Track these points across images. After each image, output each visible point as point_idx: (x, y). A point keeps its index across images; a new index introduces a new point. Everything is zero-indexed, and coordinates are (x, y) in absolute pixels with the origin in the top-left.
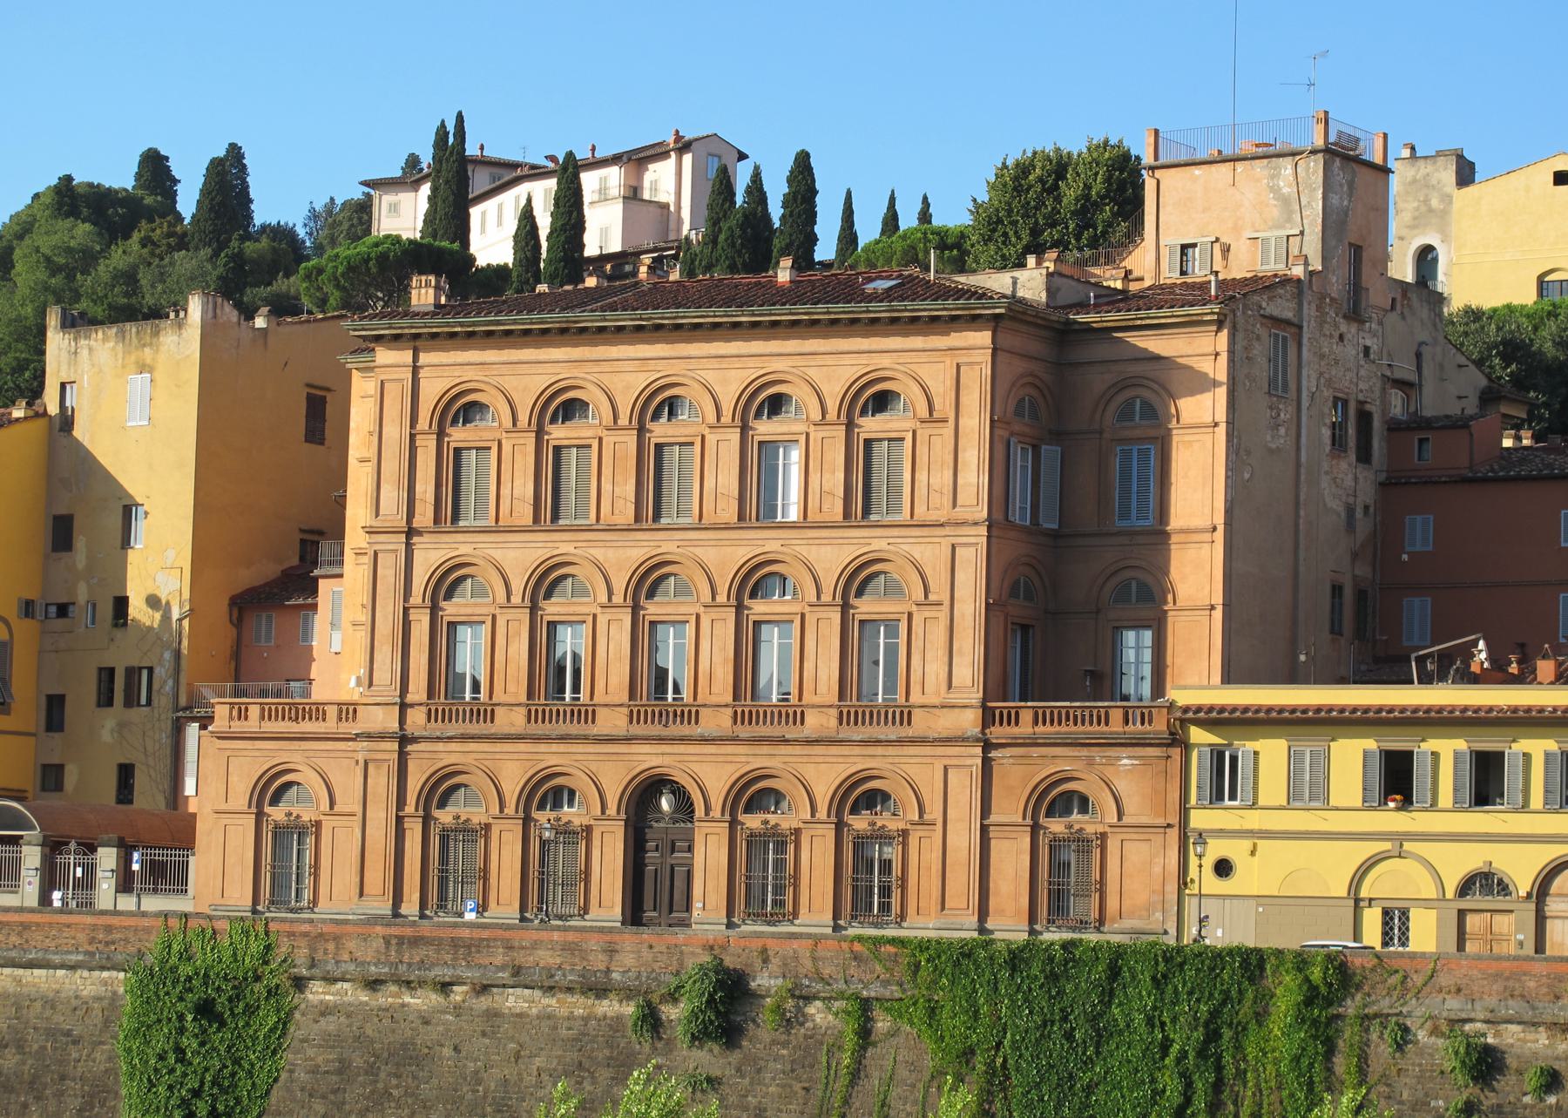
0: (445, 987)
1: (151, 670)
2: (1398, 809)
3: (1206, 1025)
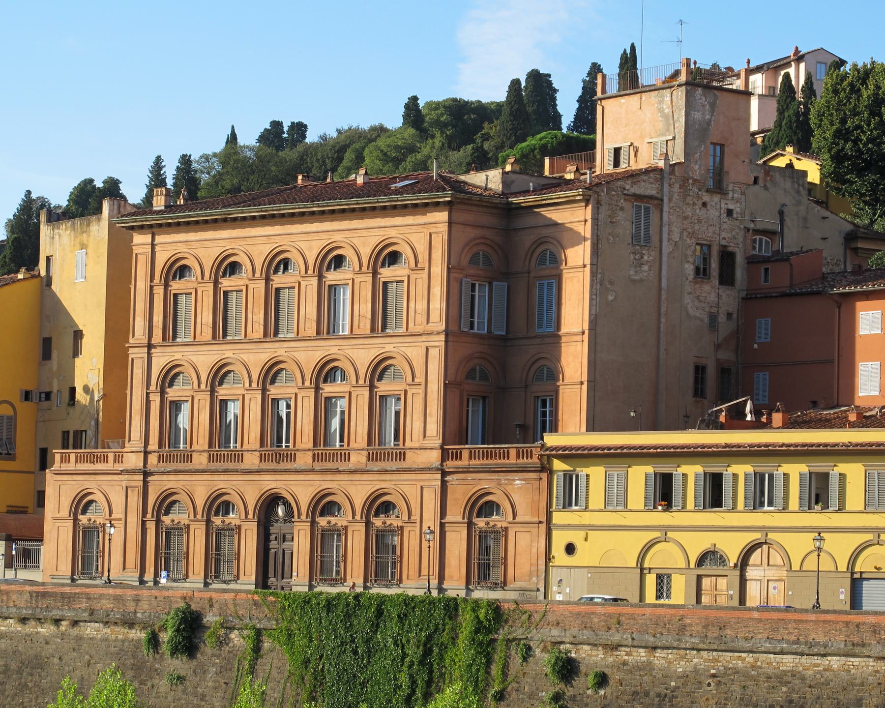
0: (57, 622)
1: (86, 431)
2: (664, 511)
3: (425, 645)
